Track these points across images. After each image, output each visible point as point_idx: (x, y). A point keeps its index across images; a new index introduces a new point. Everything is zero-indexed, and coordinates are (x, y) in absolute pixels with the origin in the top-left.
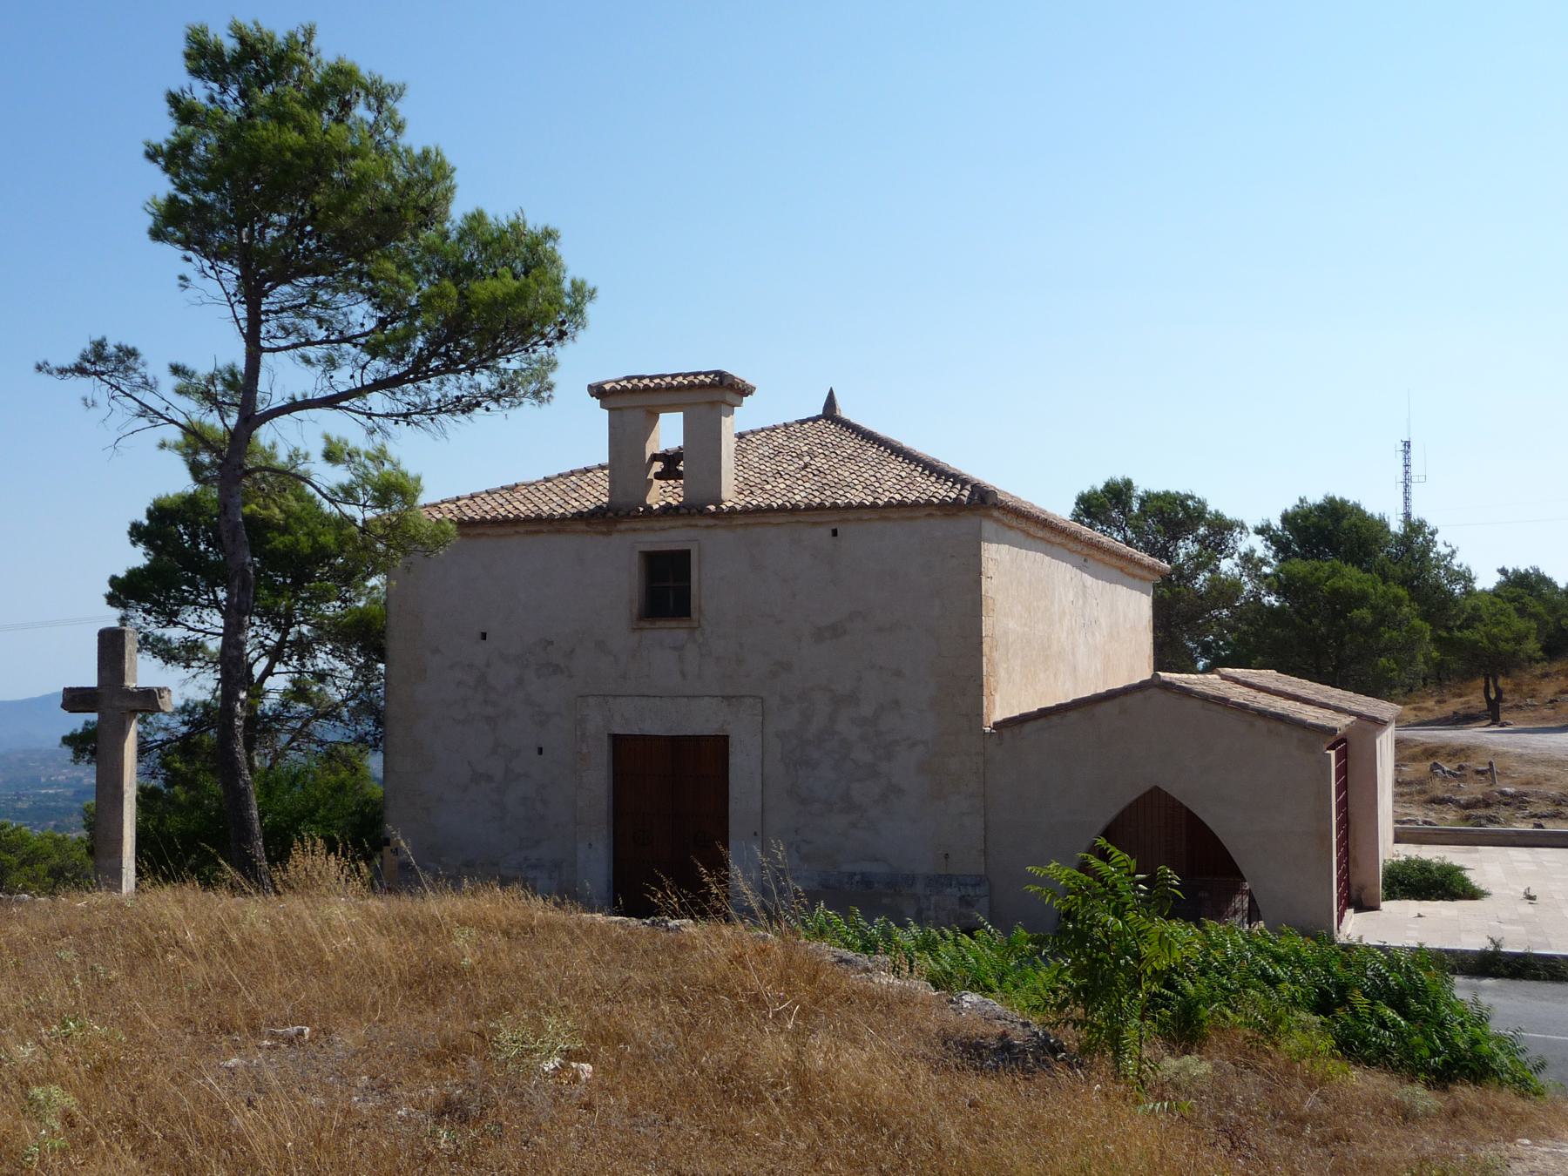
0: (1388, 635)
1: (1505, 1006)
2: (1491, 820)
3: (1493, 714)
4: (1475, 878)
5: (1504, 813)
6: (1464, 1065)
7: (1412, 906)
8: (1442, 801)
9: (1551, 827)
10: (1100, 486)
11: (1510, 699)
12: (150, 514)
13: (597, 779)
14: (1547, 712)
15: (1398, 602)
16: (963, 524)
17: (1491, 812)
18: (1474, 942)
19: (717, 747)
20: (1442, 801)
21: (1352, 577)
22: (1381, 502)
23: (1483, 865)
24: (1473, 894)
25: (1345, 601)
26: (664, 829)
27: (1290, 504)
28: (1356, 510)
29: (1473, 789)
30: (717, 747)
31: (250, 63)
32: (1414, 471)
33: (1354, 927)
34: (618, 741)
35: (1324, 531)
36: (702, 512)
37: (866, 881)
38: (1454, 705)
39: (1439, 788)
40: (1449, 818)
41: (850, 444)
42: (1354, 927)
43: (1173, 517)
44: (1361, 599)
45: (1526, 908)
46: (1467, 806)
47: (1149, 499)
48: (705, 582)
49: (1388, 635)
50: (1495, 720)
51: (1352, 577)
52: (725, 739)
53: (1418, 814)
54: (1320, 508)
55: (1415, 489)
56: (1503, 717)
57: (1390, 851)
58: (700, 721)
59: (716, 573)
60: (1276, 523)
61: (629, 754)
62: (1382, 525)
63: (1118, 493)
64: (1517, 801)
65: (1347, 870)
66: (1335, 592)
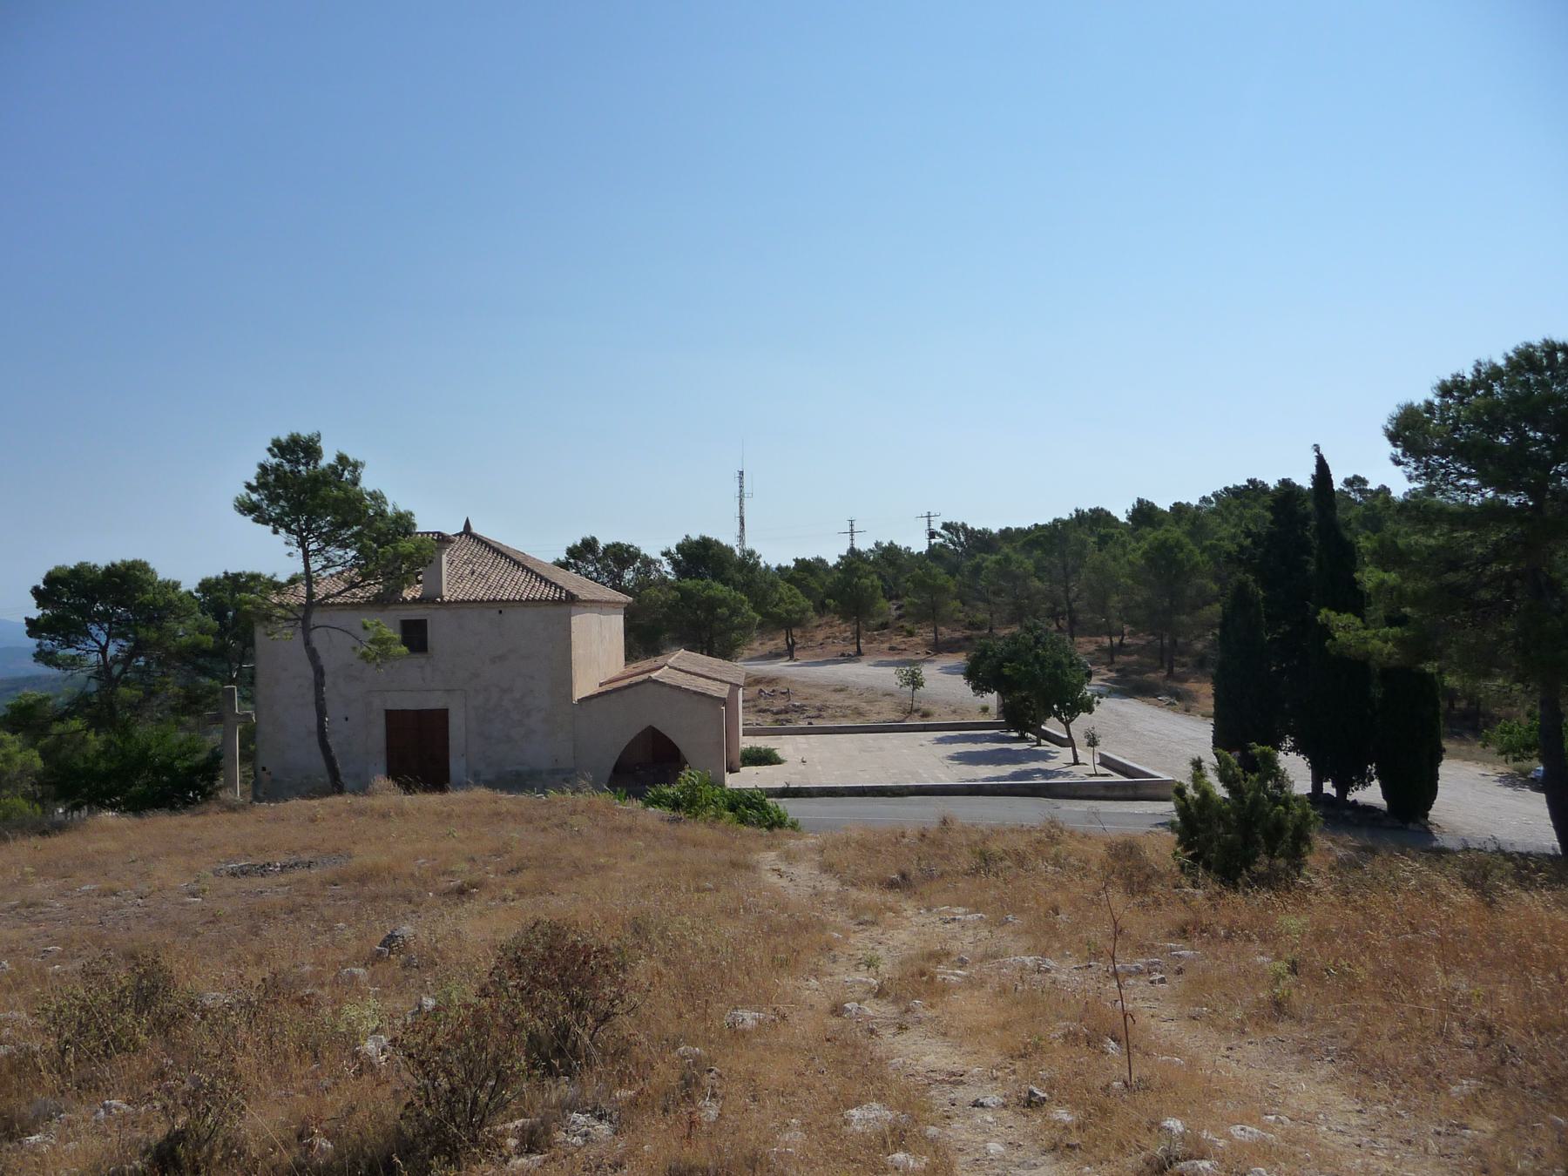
0: (737, 620)
1: (788, 806)
2: (788, 721)
3: (790, 652)
4: (779, 753)
5: (795, 716)
6: (776, 823)
7: (754, 769)
8: (764, 711)
9: (817, 723)
10: (579, 543)
11: (800, 643)
12: (45, 582)
13: (379, 732)
14: (819, 651)
15: (742, 602)
16: (563, 609)
17: (788, 716)
18: (780, 784)
19: (443, 715)
20: (764, 711)
21: (719, 589)
22: (727, 537)
23: (784, 746)
24: (779, 762)
25: (712, 604)
26: (419, 753)
27: (680, 539)
28: (717, 543)
29: (780, 704)
30: (443, 715)
31: (298, 449)
32: (745, 490)
33: (732, 781)
34: (389, 713)
35: (700, 557)
36: (434, 602)
37: (518, 774)
38: (770, 646)
39: (763, 704)
40: (767, 721)
41: (476, 548)
42: (732, 781)
43: (622, 556)
44: (723, 602)
45: (802, 767)
46: (778, 713)
47: (608, 548)
48: (434, 636)
49: (737, 620)
50: (792, 658)
51: (719, 589)
52: (446, 711)
53: (753, 719)
54: (697, 542)
55: (746, 501)
56: (796, 654)
57: (746, 743)
58: (433, 702)
59: (439, 630)
60: (673, 550)
61: (395, 719)
62: (732, 550)
63: (589, 545)
64: (800, 709)
65: (986, 861)
66: (710, 597)
